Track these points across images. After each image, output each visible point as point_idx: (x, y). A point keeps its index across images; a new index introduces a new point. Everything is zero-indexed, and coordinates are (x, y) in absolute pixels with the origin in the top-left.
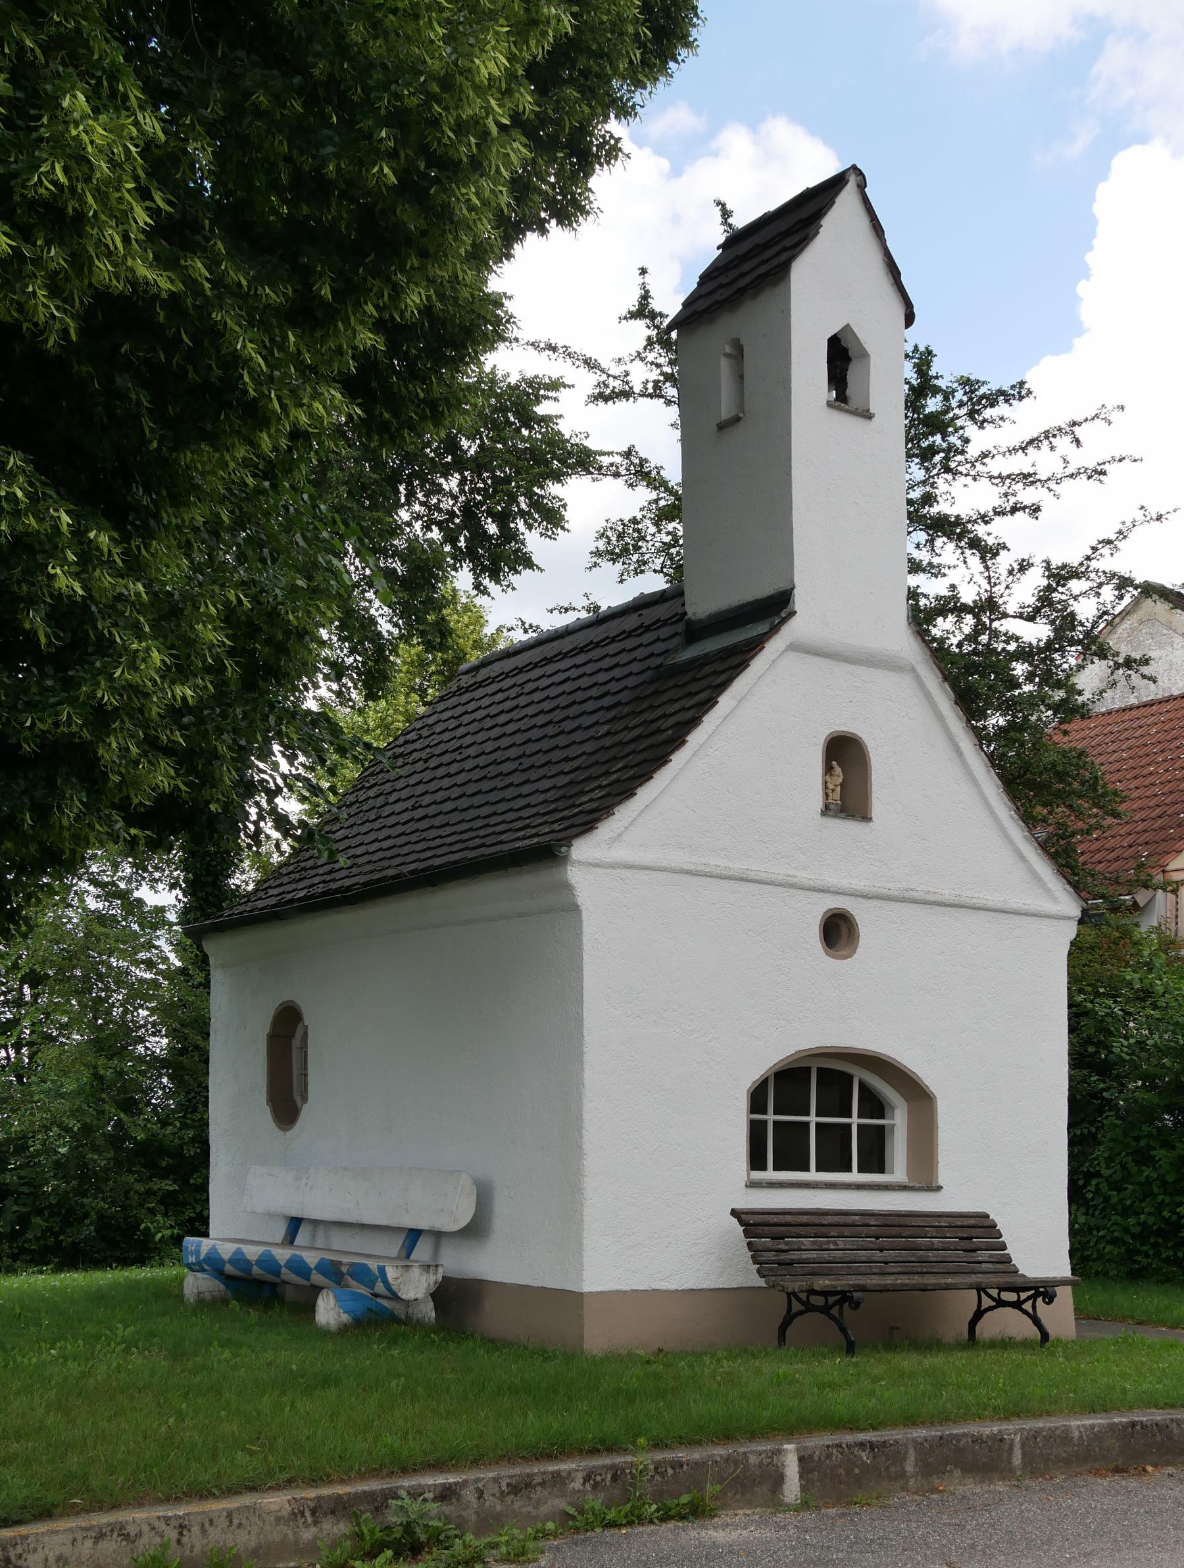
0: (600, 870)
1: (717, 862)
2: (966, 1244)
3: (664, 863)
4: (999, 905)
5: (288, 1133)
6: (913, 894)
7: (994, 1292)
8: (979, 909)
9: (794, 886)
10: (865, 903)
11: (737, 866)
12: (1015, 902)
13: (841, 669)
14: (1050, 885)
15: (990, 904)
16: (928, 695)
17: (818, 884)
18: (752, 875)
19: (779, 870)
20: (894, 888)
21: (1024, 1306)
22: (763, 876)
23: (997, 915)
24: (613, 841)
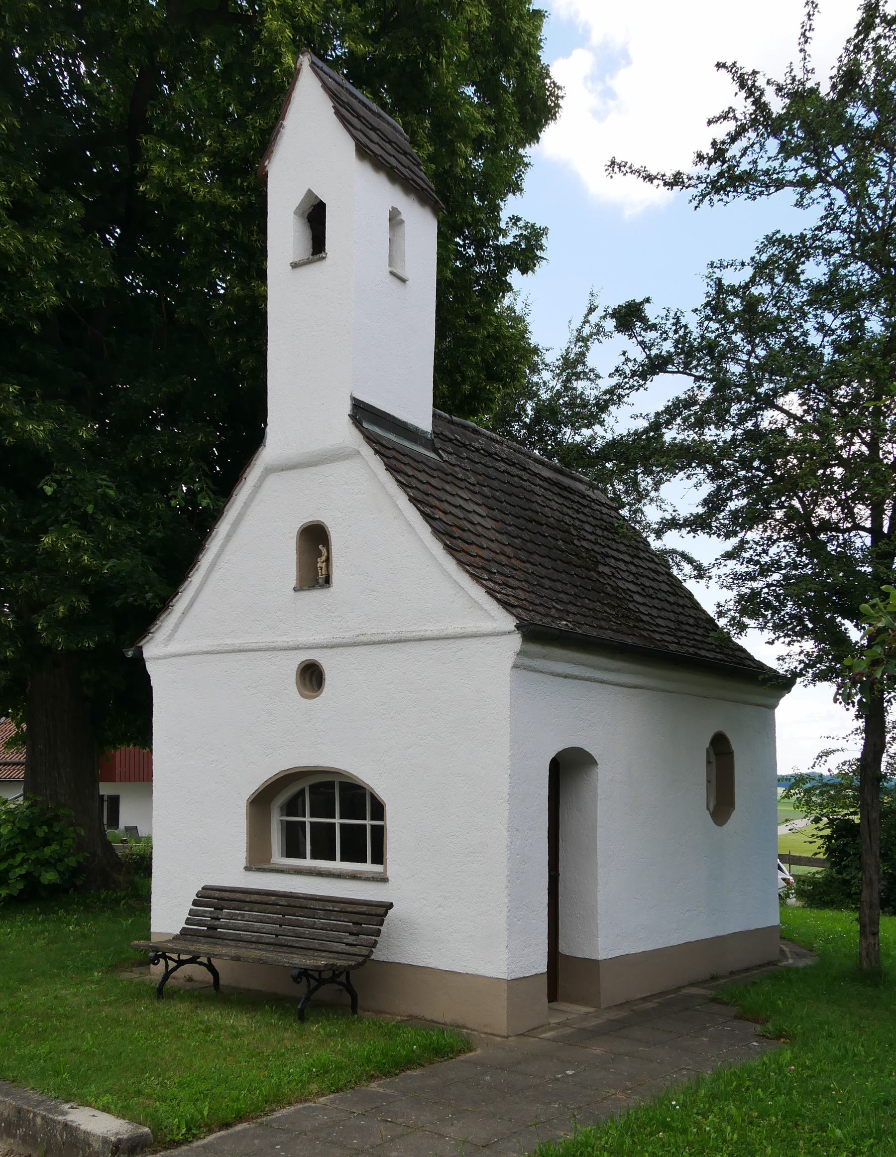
0: (160, 661)
1: (230, 641)
2: (355, 929)
3: (193, 650)
4: (436, 634)
5: (725, 826)
6: (362, 638)
7: (175, 956)
8: (420, 640)
9: (274, 649)
10: (329, 652)
11: (237, 642)
12: (471, 626)
13: (307, 473)
14: (486, 606)
15: (428, 634)
16: (247, 505)
17: (291, 644)
18: (246, 647)
19: (266, 639)
20: (348, 636)
21: (345, 981)
22: (253, 646)
23: (440, 643)
24: (171, 637)
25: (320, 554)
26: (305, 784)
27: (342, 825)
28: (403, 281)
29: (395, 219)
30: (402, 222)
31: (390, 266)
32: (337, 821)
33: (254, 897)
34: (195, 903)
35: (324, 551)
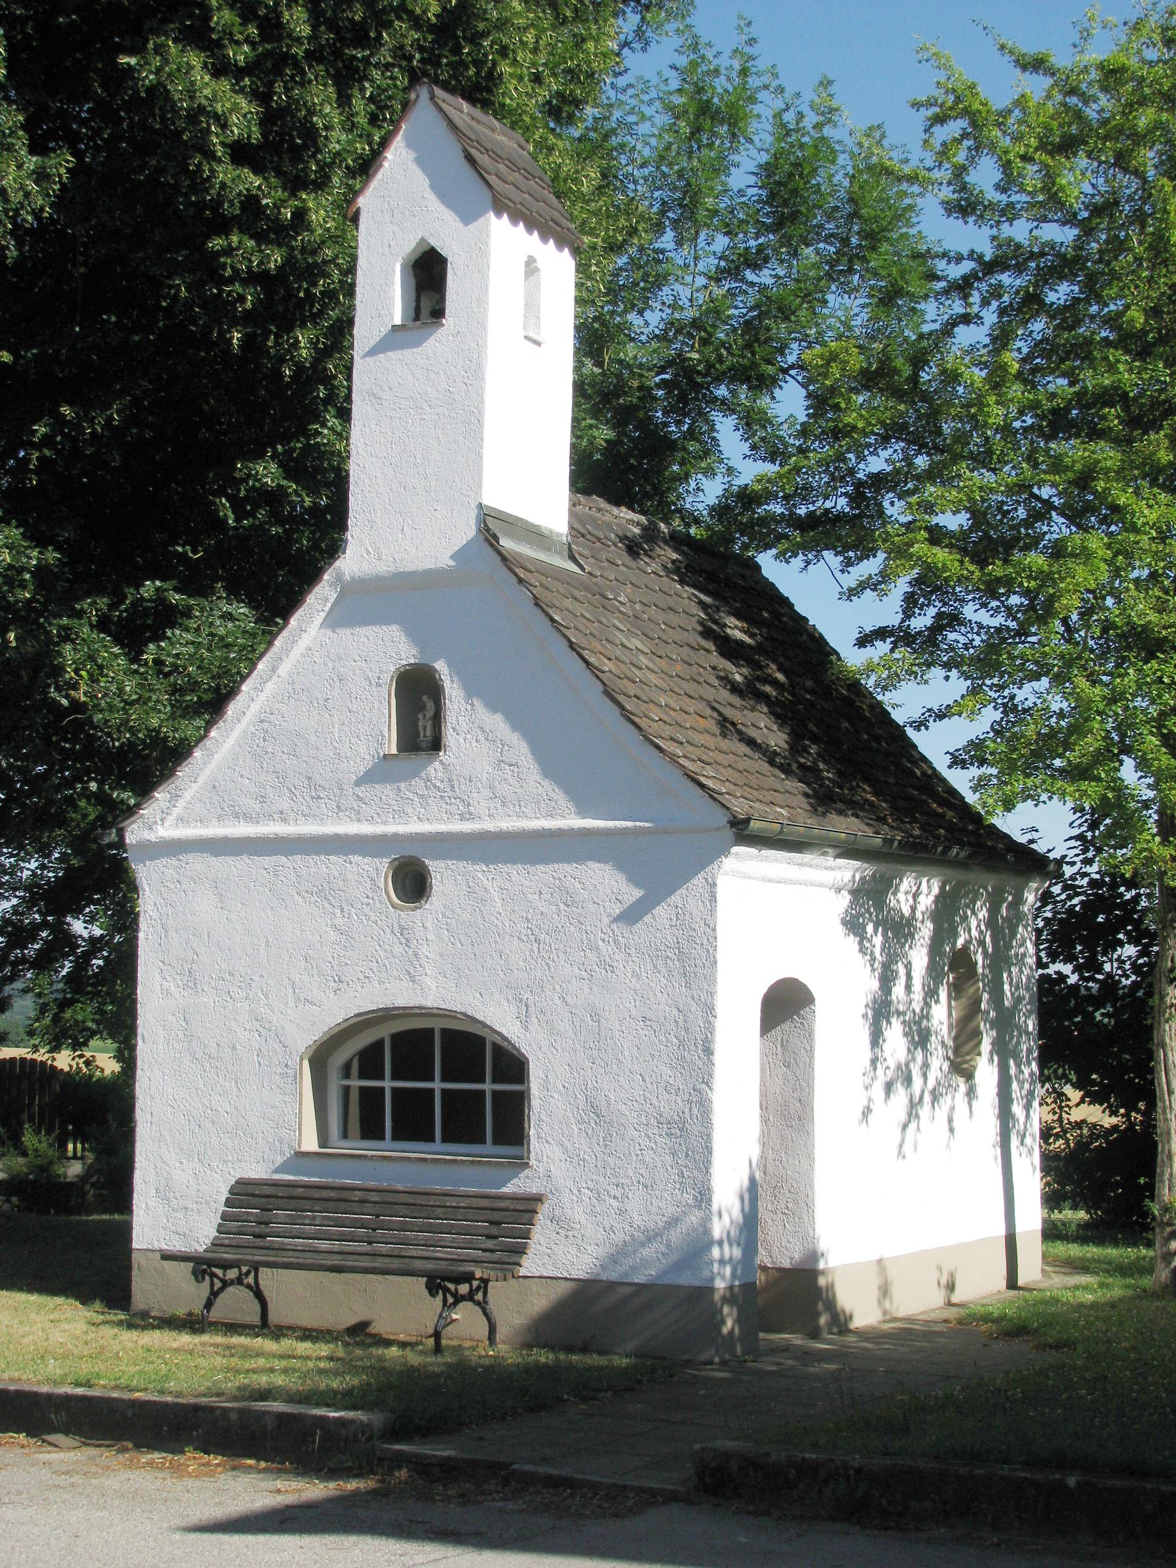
25: (422, 708)
26: (384, 1032)
27: (444, 1091)
28: (538, 343)
29: (531, 267)
30: (537, 270)
31: (525, 329)
32: (437, 1085)
33: (325, 1194)
34: (228, 1203)
35: (430, 705)
